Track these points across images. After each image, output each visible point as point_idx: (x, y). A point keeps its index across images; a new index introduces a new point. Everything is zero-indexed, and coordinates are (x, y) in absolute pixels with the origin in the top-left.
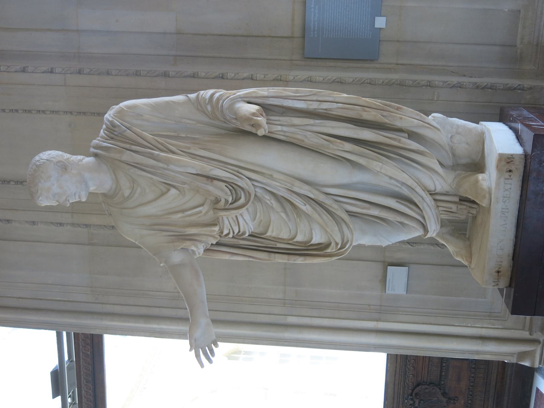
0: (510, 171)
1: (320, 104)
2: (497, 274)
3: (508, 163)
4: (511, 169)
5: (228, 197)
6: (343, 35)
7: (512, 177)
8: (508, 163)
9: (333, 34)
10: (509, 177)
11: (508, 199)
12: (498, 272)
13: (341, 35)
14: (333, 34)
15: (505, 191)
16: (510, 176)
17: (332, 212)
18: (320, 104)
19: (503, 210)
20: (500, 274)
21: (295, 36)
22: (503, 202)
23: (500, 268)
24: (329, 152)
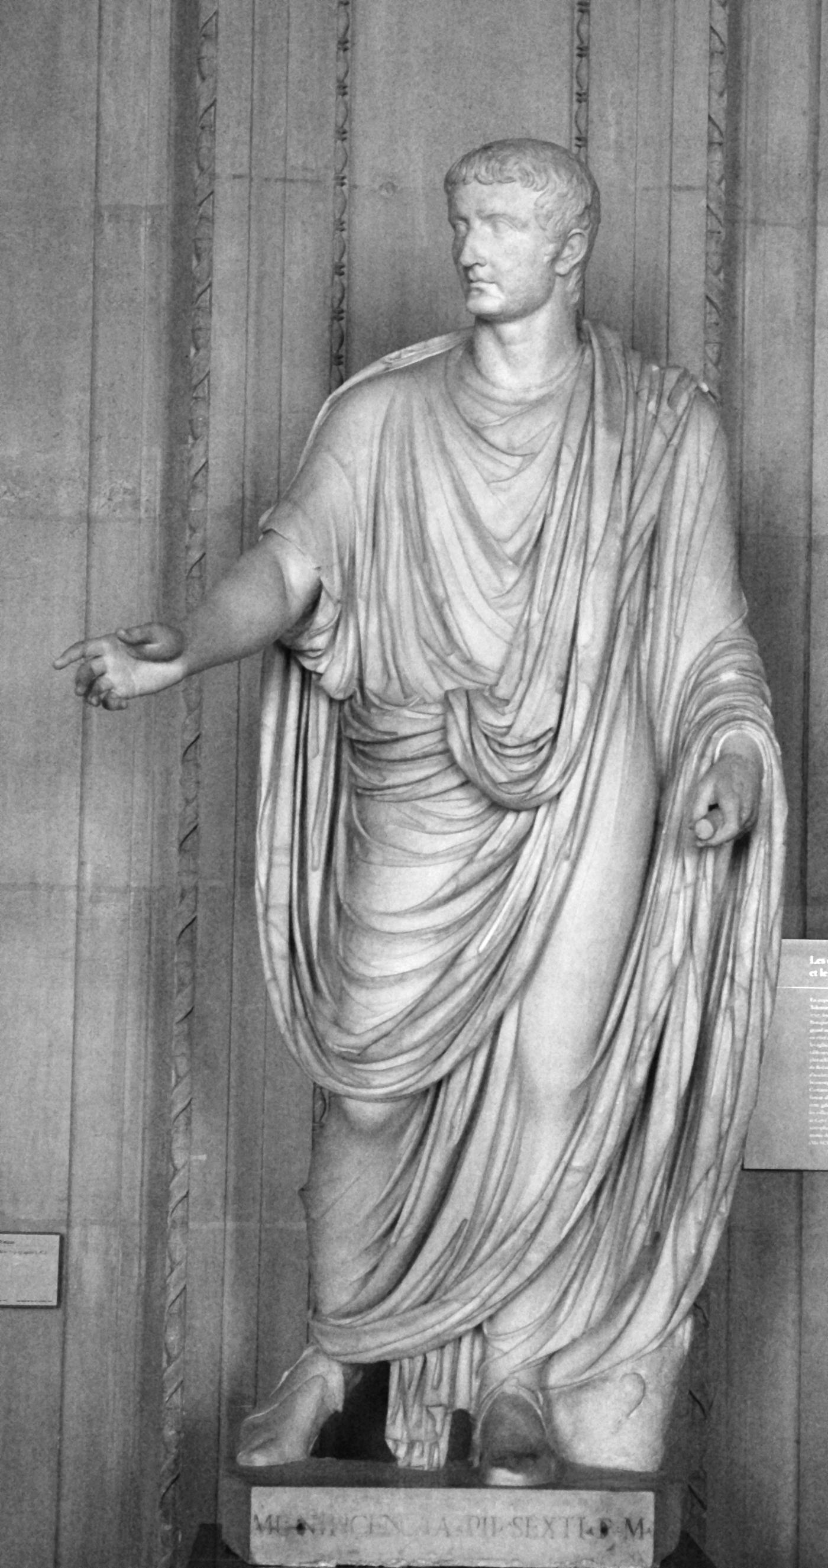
0: (604, 1530)
1: (568, 446)
2: (294, 1523)
3: (628, 1522)
4: (610, 1531)
5: (313, 662)
6: (815, 1056)
7: (588, 1537)
8: (628, 1522)
9: (819, 1026)
10: (586, 1528)
11: (522, 1534)
12: (301, 1527)
13: (817, 1053)
14: (819, 1026)
15: (546, 1521)
16: (590, 1532)
17: (639, 1149)
18: (568, 446)
19: (489, 1522)
20: (295, 1532)
21: (809, 909)
22: (514, 1519)
23: (313, 1531)
24: (308, 716)
